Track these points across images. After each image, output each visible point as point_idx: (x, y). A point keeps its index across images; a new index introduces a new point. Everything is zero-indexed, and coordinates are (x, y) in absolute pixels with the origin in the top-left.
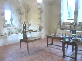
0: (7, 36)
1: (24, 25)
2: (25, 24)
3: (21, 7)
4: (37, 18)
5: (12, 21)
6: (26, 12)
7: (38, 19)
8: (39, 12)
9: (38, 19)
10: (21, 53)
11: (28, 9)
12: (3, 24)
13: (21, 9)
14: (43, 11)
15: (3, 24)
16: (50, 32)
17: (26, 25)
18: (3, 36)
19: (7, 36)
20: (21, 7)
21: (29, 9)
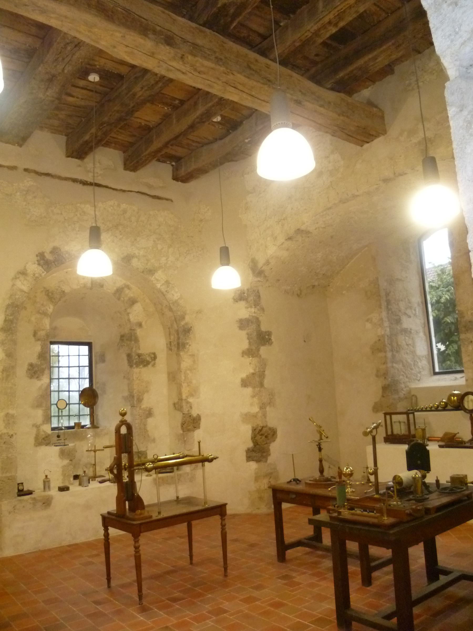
0: (54, 492)
1: (124, 430)
2: (123, 422)
3: (140, 325)
4: (238, 381)
5: (95, 403)
6: (170, 346)
7: (245, 383)
8: (245, 345)
9: (245, 383)
10: (103, 595)
11: (177, 331)
12: (37, 427)
13: (139, 332)
14: (269, 334)
15: (37, 427)
16: (102, 470)
17: (129, 427)
18: (30, 493)
19: (54, 492)
20: (140, 325)
21: (187, 331)
